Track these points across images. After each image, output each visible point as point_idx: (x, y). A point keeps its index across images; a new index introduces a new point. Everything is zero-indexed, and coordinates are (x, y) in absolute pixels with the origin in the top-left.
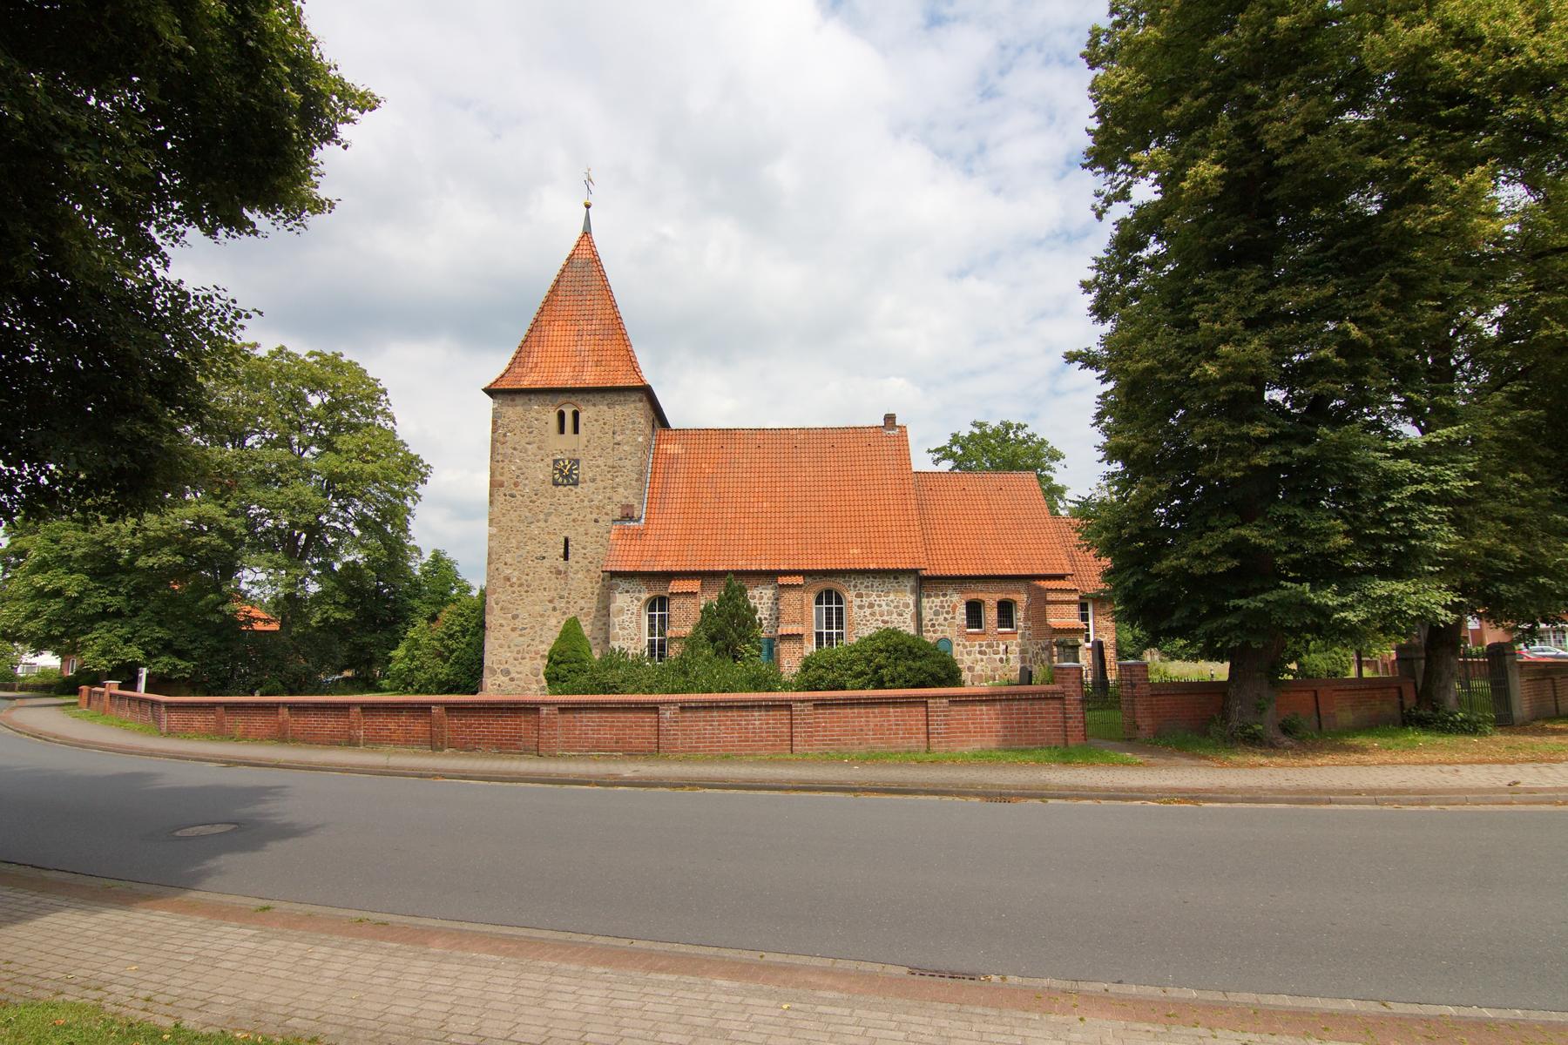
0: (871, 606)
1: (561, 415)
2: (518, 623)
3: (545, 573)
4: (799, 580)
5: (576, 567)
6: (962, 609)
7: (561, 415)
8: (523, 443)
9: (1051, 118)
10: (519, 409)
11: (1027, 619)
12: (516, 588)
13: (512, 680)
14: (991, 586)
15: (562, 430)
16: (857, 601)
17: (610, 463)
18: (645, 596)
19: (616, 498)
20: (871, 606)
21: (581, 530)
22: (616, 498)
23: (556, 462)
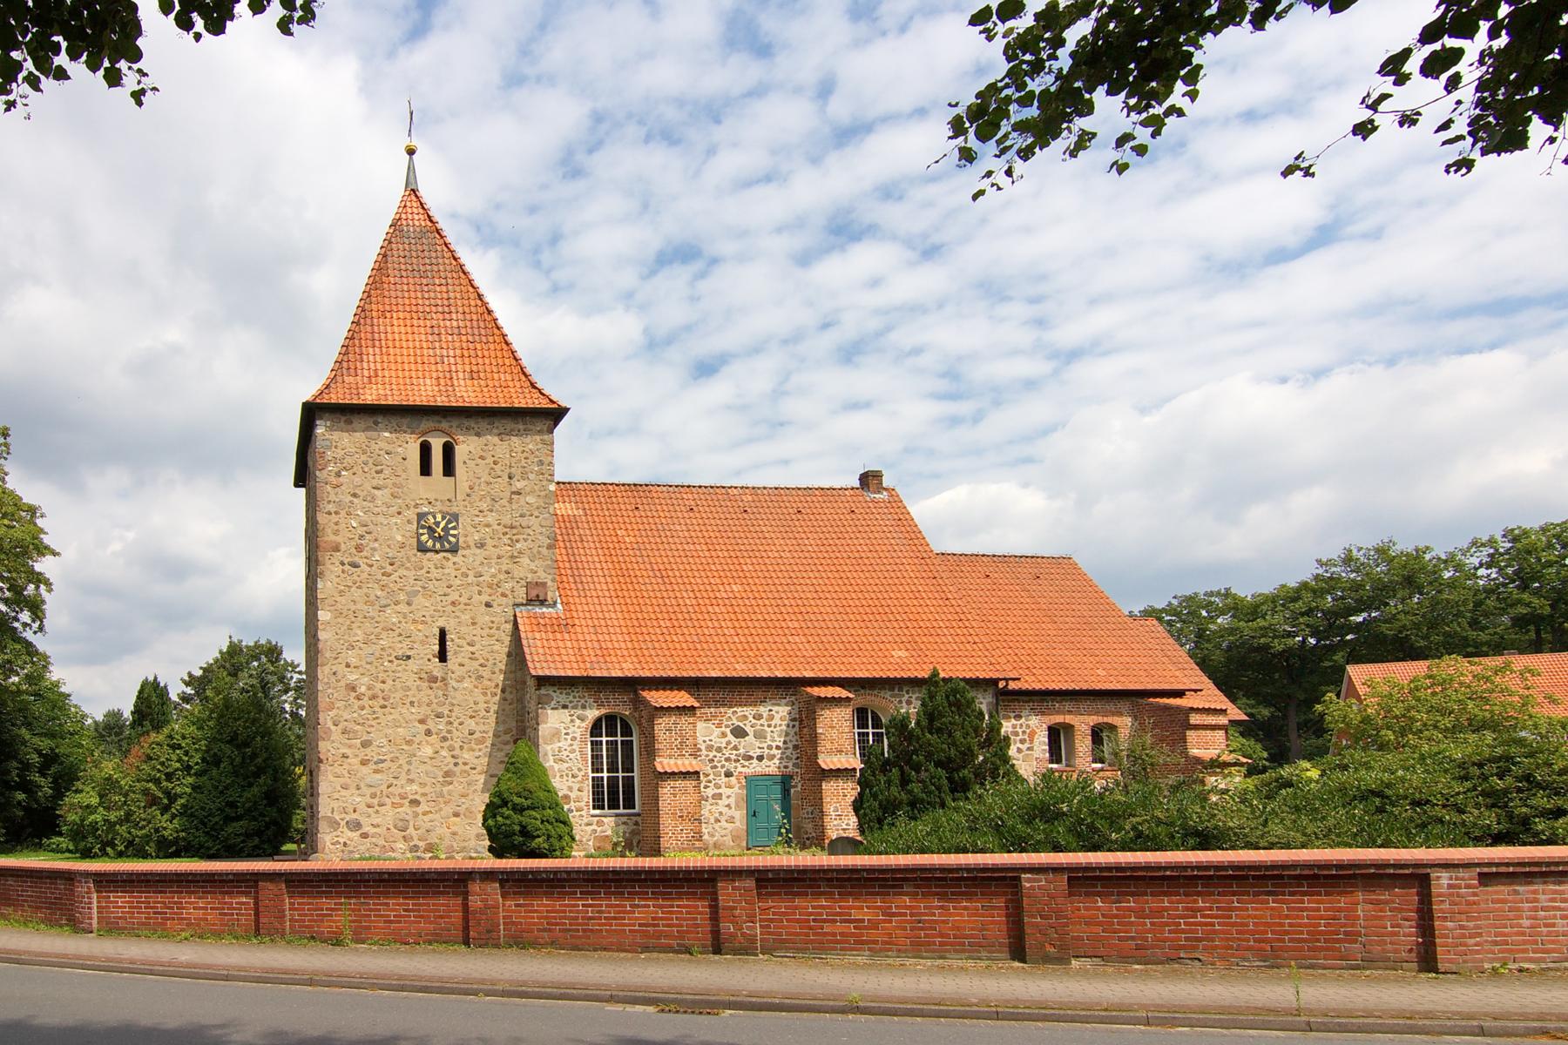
1: (425, 450)
3: (412, 681)
4: (683, 698)
5: (460, 671)
6: (1042, 738)
7: (425, 450)
9: (645, 206)
10: (360, 436)
12: (366, 702)
13: (365, 836)
14: (1083, 706)
15: (426, 469)
17: (507, 520)
18: (593, 714)
19: (518, 572)
21: (466, 617)
23: (421, 516)
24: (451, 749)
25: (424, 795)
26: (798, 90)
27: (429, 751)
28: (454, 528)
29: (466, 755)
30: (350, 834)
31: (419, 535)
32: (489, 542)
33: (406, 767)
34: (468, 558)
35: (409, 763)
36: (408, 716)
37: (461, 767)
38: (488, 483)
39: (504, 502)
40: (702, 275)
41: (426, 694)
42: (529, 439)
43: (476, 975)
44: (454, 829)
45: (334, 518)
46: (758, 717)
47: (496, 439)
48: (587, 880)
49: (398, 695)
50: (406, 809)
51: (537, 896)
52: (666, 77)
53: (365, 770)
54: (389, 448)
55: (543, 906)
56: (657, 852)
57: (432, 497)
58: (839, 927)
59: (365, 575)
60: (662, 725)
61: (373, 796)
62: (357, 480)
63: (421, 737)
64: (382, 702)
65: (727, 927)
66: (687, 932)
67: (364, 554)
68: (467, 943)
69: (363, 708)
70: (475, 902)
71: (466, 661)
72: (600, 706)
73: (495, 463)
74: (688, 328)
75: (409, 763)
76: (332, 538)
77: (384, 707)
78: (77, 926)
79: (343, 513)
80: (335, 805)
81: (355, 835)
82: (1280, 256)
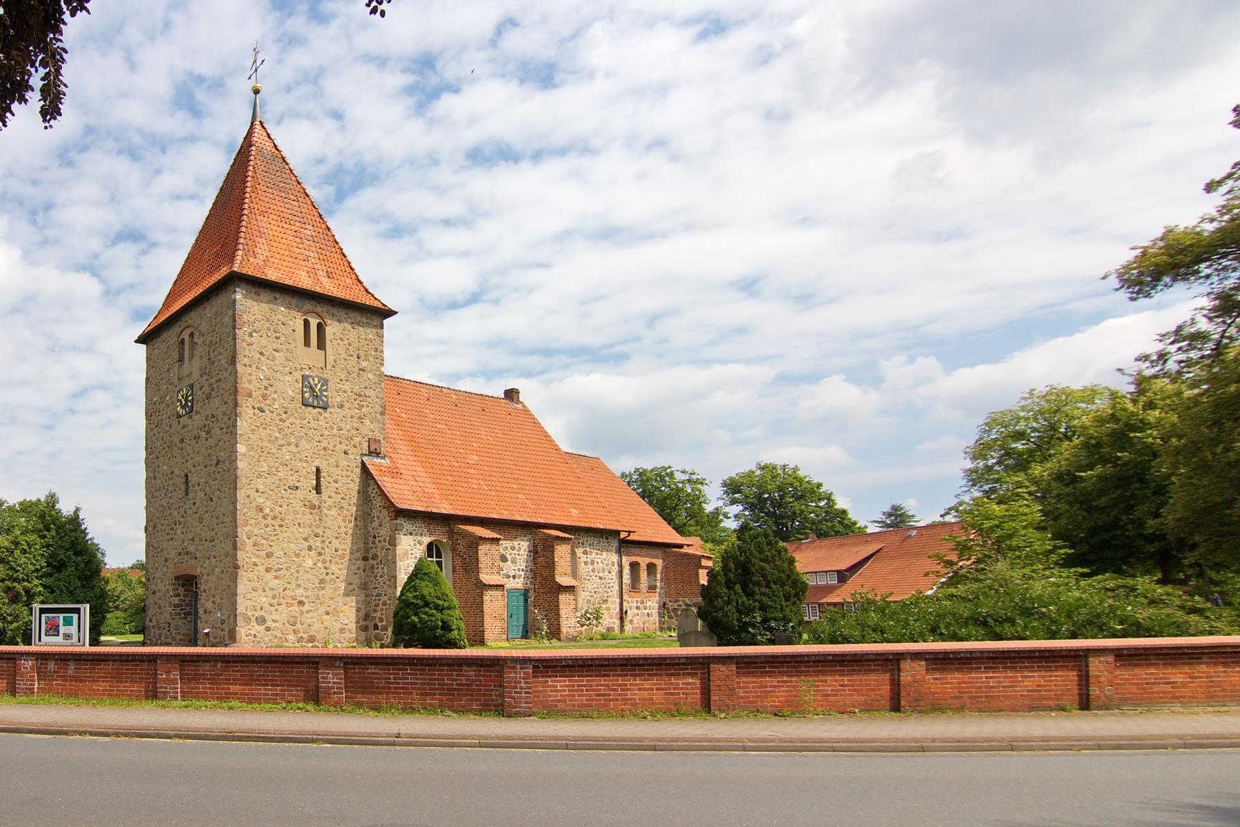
0: (592, 563)
2: (272, 562)
3: (298, 505)
5: (330, 502)
8: (270, 348)
9: (113, 199)
10: (265, 307)
12: (269, 521)
13: (268, 629)
16: (584, 558)
17: (356, 389)
18: (427, 540)
19: (364, 430)
20: (592, 563)
21: (332, 460)
22: (364, 430)
24: (324, 562)
26: (216, 144)
28: (326, 390)
30: (258, 628)
34: (334, 414)
35: (298, 572)
36: (299, 536)
39: (354, 375)
40: (144, 253)
41: (308, 518)
42: (368, 331)
45: (249, 370)
47: (349, 327)
49: (291, 517)
50: (296, 608)
51: (951, 671)
52: (135, 114)
53: (269, 576)
54: (283, 319)
55: (954, 678)
58: (1162, 687)
59: (268, 419)
60: (483, 549)
61: (274, 597)
63: (305, 552)
65: (1094, 691)
67: (268, 402)
69: (267, 526)
70: (905, 677)
71: (333, 494)
72: (431, 534)
74: (132, 286)
76: (247, 386)
77: (281, 526)
80: (249, 603)
81: (261, 628)
82: (454, 305)
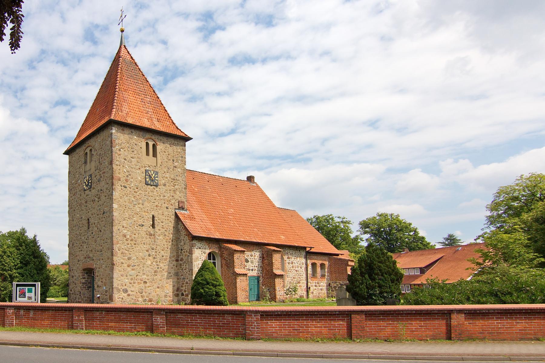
0: (292, 263)
1: (147, 144)
2: (130, 262)
3: (143, 234)
5: (159, 232)
7: (147, 144)
8: (129, 156)
11: (328, 272)
12: (129, 242)
13: (129, 295)
14: (319, 257)
17: (172, 177)
18: (208, 251)
19: (176, 197)
21: (160, 212)
22: (176, 197)
24: (157, 262)
25: (148, 279)
27: (149, 262)
28: (157, 177)
29: (161, 265)
30: (124, 294)
31: (146, 178)
32: (167, 184)
33: (142, 268)
34: (161, 189)
35: (143, 267)
37: (160, 269)
38: (167, 162)
39: (171, 170)
41: (148, 240)
42: (178, 148)
43: (295, 350)
44: (158, 293)
46: (251, 256)
47: (169, 146)
48: (498, 313)
49: (140, 240)
50: (142, 285)
51: (478, 319)
52: (65, 43)
53: (129, 269)
54: (136, 143)
55: (480, 323)
56: (236, 303)
57: (150, 164)
59: (128, 192)
60: (236, 256)
61: (132, 279)
62: (126, 153)
63: (147, 257)
64: (135, 242)
66: (537, 332)
67: (128, 183)
68: (351, 338)
70: (454, 322)
71: (161, 229)
73: (169, 155)
74: (63, 127)
75: (143, 267)
76: (118, 175)
77: (135, 244)
78: (245, 337)
79: (121, 166)
80: (119, 282)
81: (126, 295)
82: (222, 135)
